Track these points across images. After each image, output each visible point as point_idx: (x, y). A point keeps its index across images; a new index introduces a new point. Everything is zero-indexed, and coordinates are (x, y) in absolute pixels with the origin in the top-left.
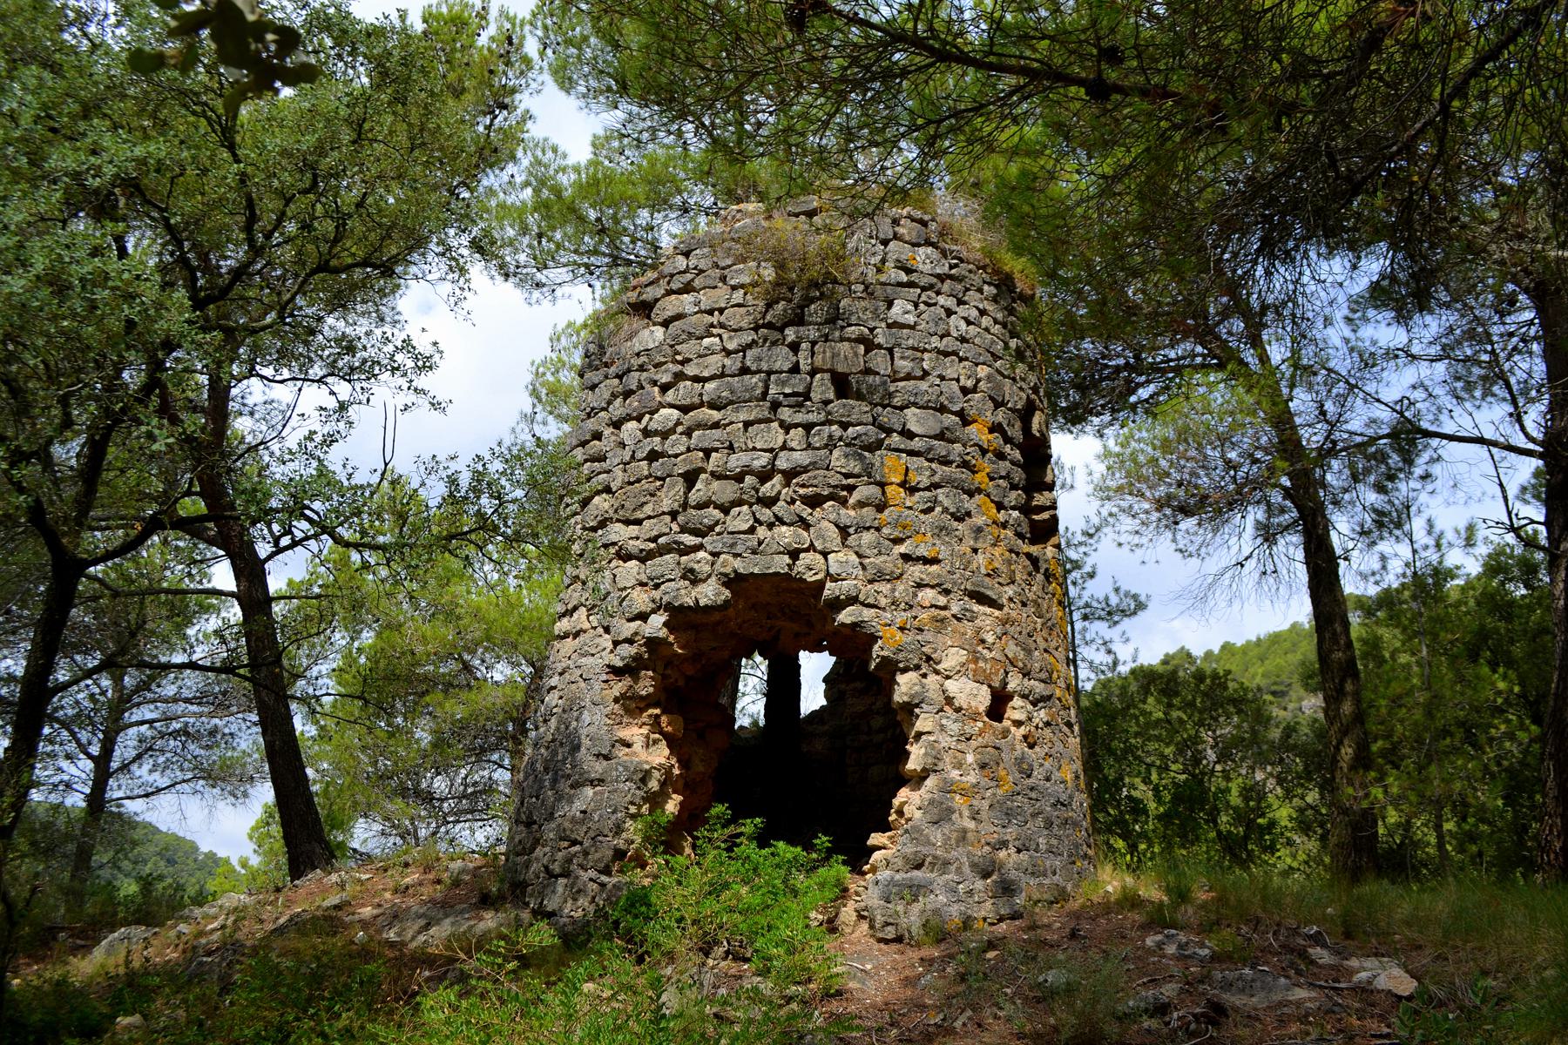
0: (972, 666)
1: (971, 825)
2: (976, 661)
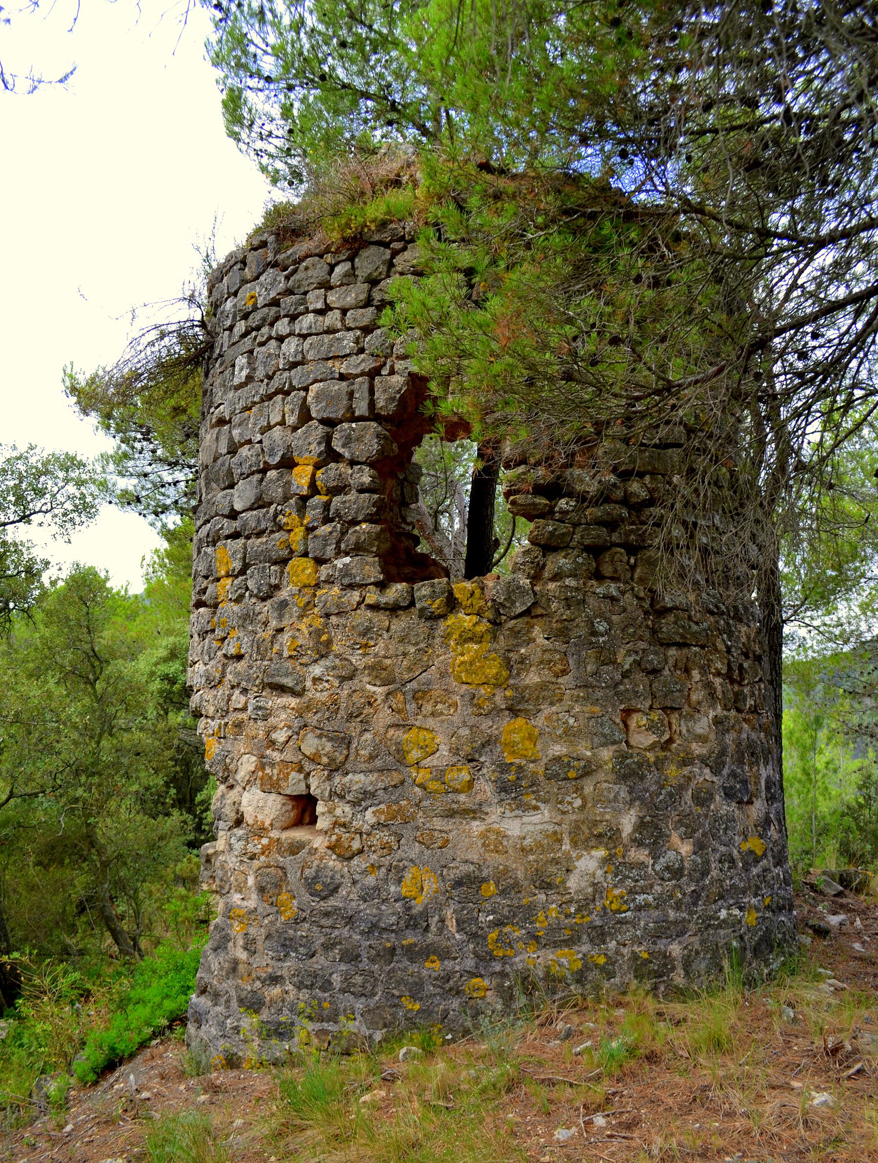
0: (260, 774)
1: (242, 955)
2: (263, 768)
